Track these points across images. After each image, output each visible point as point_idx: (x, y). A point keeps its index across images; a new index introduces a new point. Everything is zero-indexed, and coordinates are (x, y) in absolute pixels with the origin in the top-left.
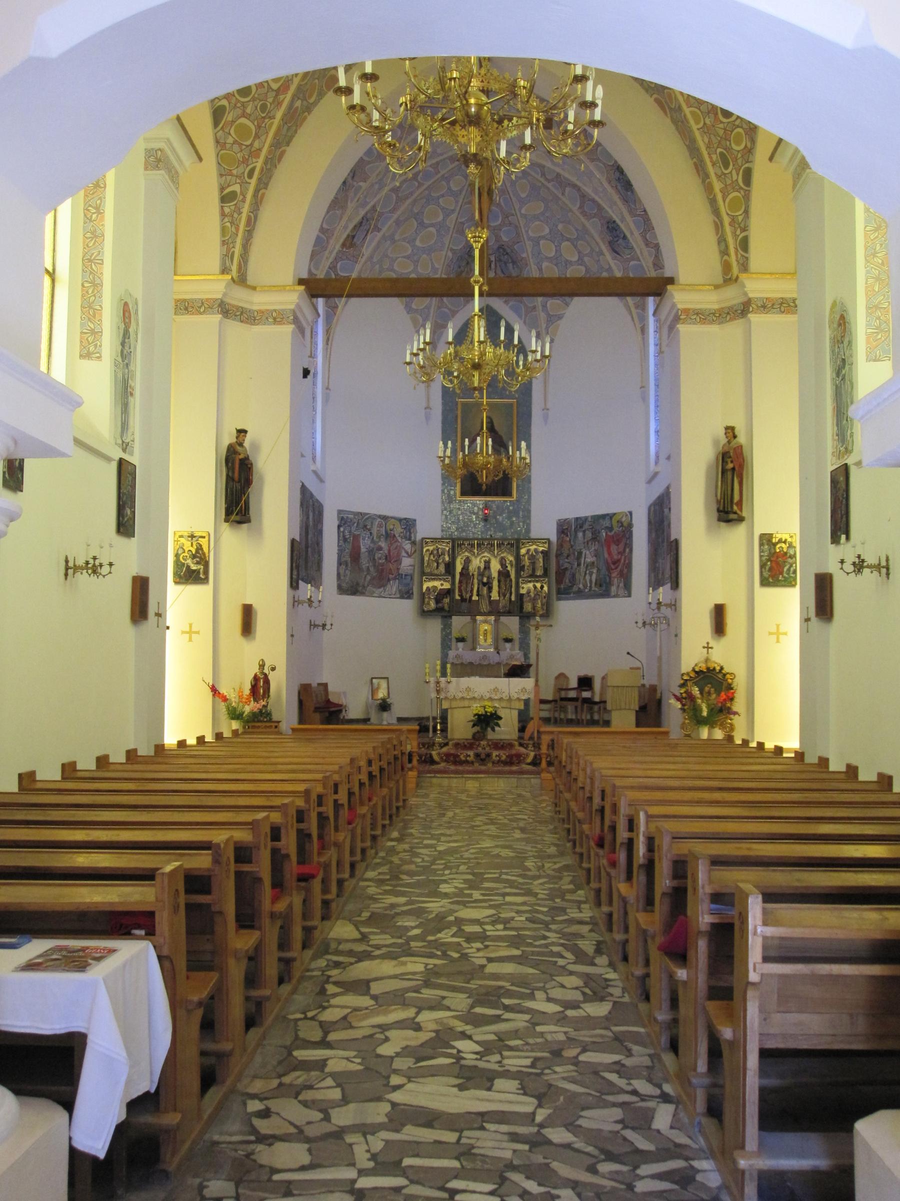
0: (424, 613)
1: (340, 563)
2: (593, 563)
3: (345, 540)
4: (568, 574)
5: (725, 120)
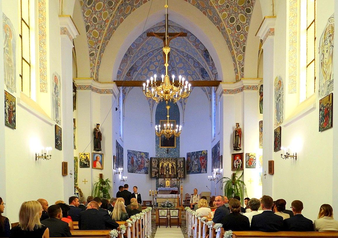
0: (151, 177)
1: (128, 165)
2: (197, 164)
3: (130, 158)
4: (190, 167)
5: (238, 32)
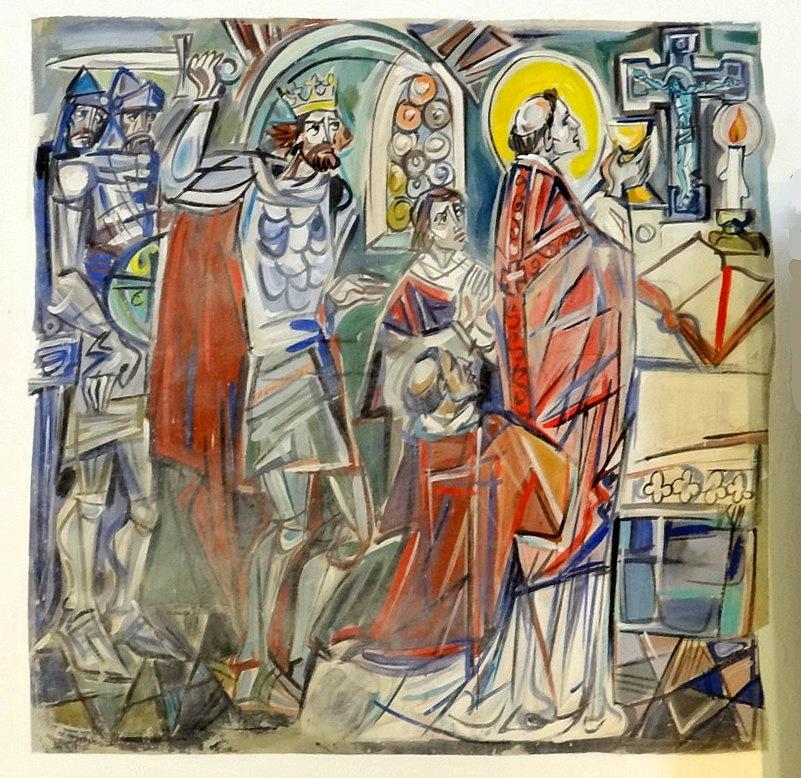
1: (57, 479)
3: (105, 271)
